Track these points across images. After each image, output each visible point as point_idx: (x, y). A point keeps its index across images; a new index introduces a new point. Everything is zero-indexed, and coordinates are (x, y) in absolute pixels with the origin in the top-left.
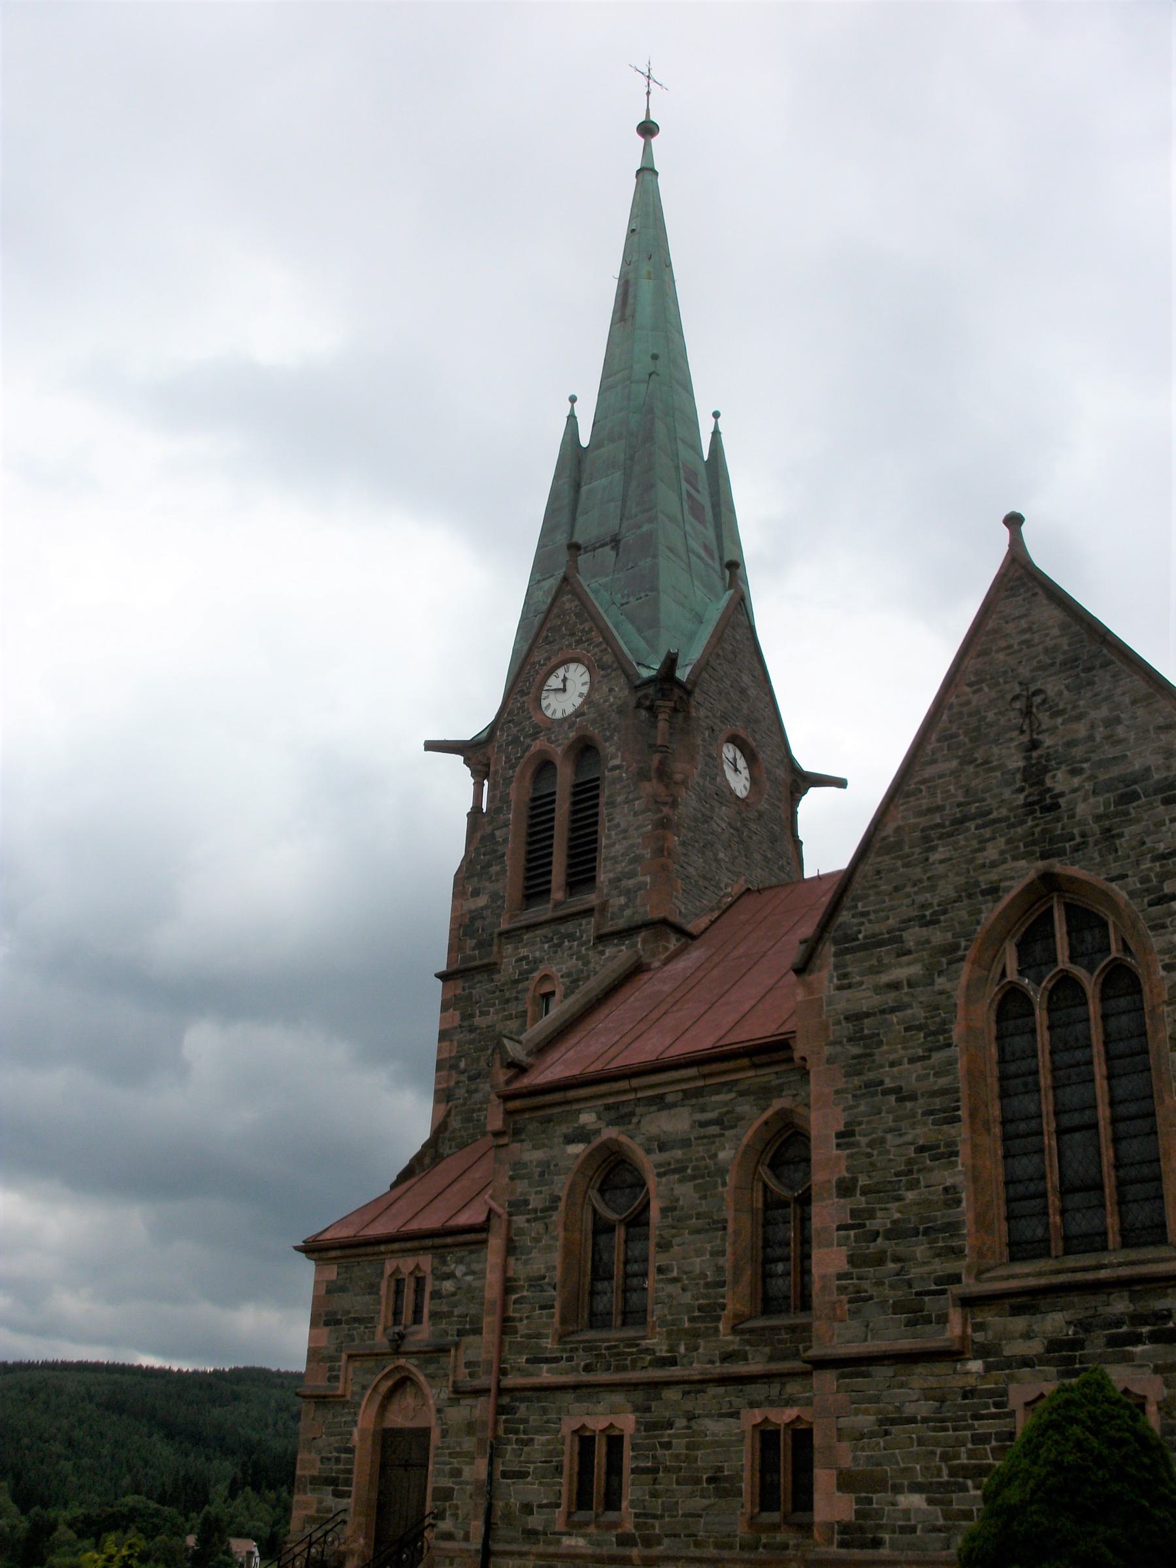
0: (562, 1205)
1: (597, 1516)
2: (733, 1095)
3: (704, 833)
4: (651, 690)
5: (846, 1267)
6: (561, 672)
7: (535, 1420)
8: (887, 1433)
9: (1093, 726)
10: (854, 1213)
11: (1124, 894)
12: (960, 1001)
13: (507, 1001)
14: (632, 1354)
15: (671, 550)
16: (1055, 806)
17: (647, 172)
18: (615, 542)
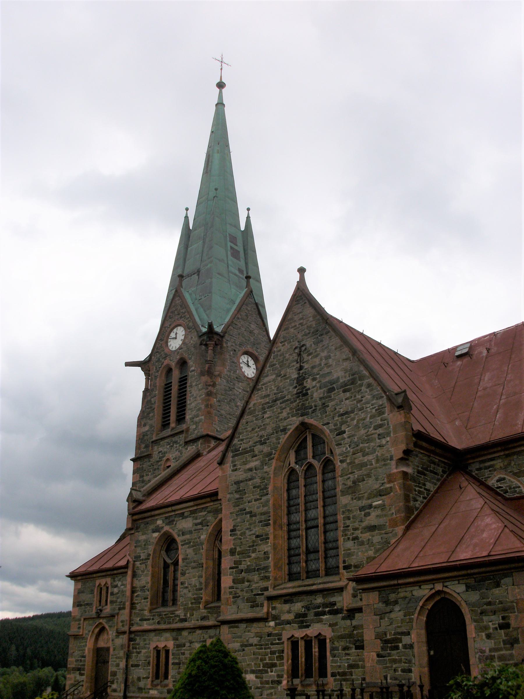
0: (151, 557)
1: (161, 682)
2: (206, 513)
3: (230, 395)
4: (205, 337)
5: (232, 584)
6: (175, 330)
7: (142, 644)
8: (244, 650)
9: (321, 360)
10: (235, 562)
11: (328, 431)
12: (272, 476)
13: (155, 470)
14: (172, 617)
15: (219, 274)
16: (307, 394)
17: (220, 105)
18: (198, 272)
